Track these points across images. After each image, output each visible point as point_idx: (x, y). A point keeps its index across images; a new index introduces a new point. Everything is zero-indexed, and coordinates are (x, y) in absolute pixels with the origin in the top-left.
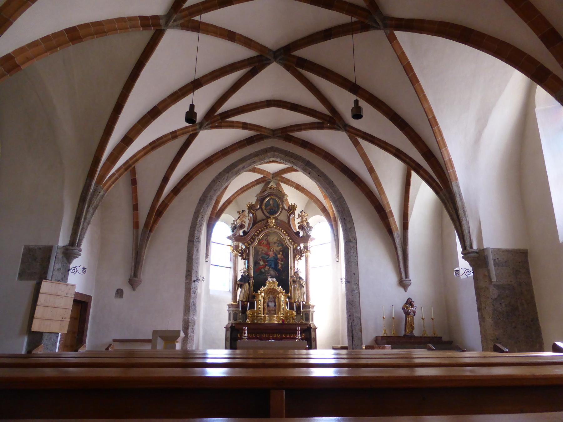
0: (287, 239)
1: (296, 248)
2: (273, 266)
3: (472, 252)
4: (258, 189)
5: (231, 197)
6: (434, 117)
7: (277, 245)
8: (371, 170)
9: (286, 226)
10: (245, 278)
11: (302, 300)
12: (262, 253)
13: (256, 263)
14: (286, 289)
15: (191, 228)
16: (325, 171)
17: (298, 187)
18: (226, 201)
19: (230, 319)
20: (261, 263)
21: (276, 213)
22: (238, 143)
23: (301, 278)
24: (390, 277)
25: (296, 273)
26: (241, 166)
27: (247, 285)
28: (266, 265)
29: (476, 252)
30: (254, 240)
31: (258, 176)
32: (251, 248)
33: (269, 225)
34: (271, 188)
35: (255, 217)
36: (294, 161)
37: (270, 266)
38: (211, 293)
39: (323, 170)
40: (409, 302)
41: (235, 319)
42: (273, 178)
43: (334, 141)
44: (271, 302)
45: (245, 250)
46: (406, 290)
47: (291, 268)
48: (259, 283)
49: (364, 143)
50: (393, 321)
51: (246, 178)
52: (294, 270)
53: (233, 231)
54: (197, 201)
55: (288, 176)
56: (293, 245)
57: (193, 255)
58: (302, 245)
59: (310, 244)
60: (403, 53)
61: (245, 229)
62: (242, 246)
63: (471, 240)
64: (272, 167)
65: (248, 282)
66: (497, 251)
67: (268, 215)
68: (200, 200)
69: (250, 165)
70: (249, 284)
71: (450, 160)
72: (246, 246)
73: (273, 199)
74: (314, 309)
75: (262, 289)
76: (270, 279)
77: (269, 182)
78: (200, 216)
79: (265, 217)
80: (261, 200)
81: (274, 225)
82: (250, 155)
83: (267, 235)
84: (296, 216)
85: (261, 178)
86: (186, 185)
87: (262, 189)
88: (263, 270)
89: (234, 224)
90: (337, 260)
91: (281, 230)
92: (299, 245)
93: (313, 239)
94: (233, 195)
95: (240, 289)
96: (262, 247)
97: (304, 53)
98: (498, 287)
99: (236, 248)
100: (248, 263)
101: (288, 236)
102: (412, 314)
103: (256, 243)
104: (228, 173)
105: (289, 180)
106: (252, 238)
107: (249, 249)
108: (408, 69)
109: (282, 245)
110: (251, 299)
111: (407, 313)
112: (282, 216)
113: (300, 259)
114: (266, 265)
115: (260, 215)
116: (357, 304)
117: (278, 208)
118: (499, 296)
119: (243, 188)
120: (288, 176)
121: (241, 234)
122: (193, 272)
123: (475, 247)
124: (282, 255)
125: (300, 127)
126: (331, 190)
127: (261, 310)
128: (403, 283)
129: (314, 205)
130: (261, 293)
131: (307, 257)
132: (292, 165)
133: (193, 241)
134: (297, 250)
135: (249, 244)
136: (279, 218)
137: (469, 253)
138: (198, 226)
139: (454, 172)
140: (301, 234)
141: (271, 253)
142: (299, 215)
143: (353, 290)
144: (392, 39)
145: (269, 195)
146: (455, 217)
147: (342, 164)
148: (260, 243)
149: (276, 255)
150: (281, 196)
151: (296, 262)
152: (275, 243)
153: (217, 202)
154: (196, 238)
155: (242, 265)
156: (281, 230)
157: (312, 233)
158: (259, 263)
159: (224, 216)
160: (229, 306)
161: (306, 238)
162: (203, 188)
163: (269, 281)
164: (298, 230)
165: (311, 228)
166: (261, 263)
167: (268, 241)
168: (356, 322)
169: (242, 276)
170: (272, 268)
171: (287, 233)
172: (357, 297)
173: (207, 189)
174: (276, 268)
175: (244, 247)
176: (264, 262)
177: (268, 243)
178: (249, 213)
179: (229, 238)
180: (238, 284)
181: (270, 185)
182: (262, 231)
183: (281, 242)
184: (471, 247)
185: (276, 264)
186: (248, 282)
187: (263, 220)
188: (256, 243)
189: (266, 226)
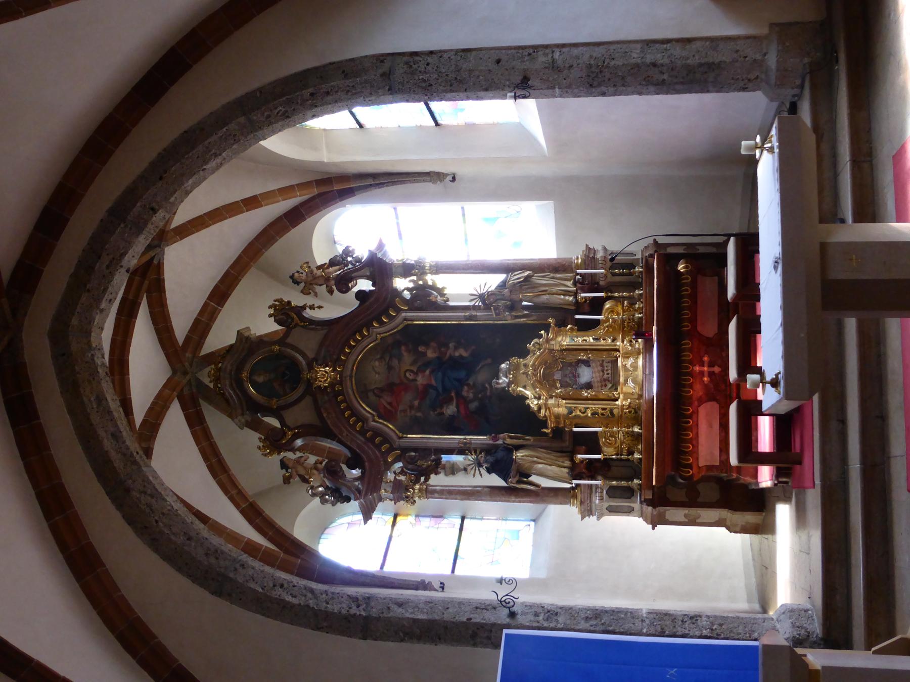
0: (379, 331)
1: (405, 301)
2: (462, 374)
4: (218, 423)
5: (237, 505)
7: (395, 362)
10: (500, 463)
11: (570, 283)
12: (419, 409)
14: (532, 331)
15: (319, 628)
16: (150, 153)
17: (220, 294)
18: (251, 522)
19: (629, 511)
20: (450, 410)
21: (295, 364)
22: (24, 454)
23: (503, 285)
25: (487, 300)
26: (108, 444)
27: (519, 454)
28: (459, 394)
30: (377, 433)
31: (175, 416)
33: (332, 385)
34: (217, 380)
35: (306, 431)
37: (461, 382)
38: (542, 574)
39: (144, 165)
41: (628, 493)
42: (185, 373)
44: (576, 376)
45: (409, 462)
47: (470, 318)
48: (526, 422)
51: (177, 465)
52: (474, 308)
53: (348, 500)
54: (223, 605)
55: (181, 327)
56: (399, 311)
57: (415, 621)
58: (401, 284)
59: (395, 254)
62: (395, 471)
64: (146, 367)
67: (300, 390)
68: (218, 593)
69: (110, 412)
70: (518, 448)
73: (252, 373)
74: (598, 247)
75: (533, 404)
76: (503, 380)
77: (200, 383)
78: (278, 593)
79: (308, 399)
80: (249, 412)
81: (334, 370)
82: (71, 412)
83: (364, 393)
84: (308, 300)
85: (184, 408)
86: (160, 645)
87: (217, 407)
88: (474, 406)
89: (322, 496)
90: (450, 178)
91: (351, 347)
92: (397, 293)
93: (381, 246)
94: (232, 499)
95: (533, 478)
96: (401, 407)
99: (401, 493)
101: (369, 325)
104: (128, 490)
105: (197, 322)
106: (371, 440)
107: (405, 450)
109: (398, 344)
110: (567, 442)
112: (308, 343)
113: (440, 292)
114: (459, 394)
115: (301, 414)
116: (598, 52)
117: (280, 356)
119: (211, 468)
120: (181, 327)
121: (356, 472)
122: (477, 618)
124: (427, 345)
126: (214, 138)
127: (597, 406)
129: (277, 250)
130: (547, 408)
131: (439, 269)
132: (123, 270)
133: (367, 619)
134: (414, 297)
135: (391, 449)
136: (311, 355)
138: (312, 603)
140: (365, 285)
141: (421, 380)
142: (305, 292)
143: (553, 66)
145: (239, 384)
146: (370, 181)
148: (388, 415)
149: (427, 364)
150: (247, 344)
151: (451, 304)
152: (390, 368)
153: (250, 548)
154: (354, 610)
156: (351, 347)
157: (362, 252)
158: (452, 418)
159: (300, 533)
160: (587, 511)
161: (378, 268)
162: (180, 583)
163: (509, 384)
165: (347, 252)
166: (450, 410)
167: (382, 390)
168: (659, 58)
169: (489, 471)
170: (468, 376)
172: (576, 51)
173: (179, 570)
175: (399, 465)
176: (449, 401)
177: (391, 388)
178: (293, 450)
179: (367, 515)
180: (516, 487)
181: (206, 381)
182: (349, 407)
183: (388, 349)
185: (456, 363)
187: (315, 401)
189: (335, 391)
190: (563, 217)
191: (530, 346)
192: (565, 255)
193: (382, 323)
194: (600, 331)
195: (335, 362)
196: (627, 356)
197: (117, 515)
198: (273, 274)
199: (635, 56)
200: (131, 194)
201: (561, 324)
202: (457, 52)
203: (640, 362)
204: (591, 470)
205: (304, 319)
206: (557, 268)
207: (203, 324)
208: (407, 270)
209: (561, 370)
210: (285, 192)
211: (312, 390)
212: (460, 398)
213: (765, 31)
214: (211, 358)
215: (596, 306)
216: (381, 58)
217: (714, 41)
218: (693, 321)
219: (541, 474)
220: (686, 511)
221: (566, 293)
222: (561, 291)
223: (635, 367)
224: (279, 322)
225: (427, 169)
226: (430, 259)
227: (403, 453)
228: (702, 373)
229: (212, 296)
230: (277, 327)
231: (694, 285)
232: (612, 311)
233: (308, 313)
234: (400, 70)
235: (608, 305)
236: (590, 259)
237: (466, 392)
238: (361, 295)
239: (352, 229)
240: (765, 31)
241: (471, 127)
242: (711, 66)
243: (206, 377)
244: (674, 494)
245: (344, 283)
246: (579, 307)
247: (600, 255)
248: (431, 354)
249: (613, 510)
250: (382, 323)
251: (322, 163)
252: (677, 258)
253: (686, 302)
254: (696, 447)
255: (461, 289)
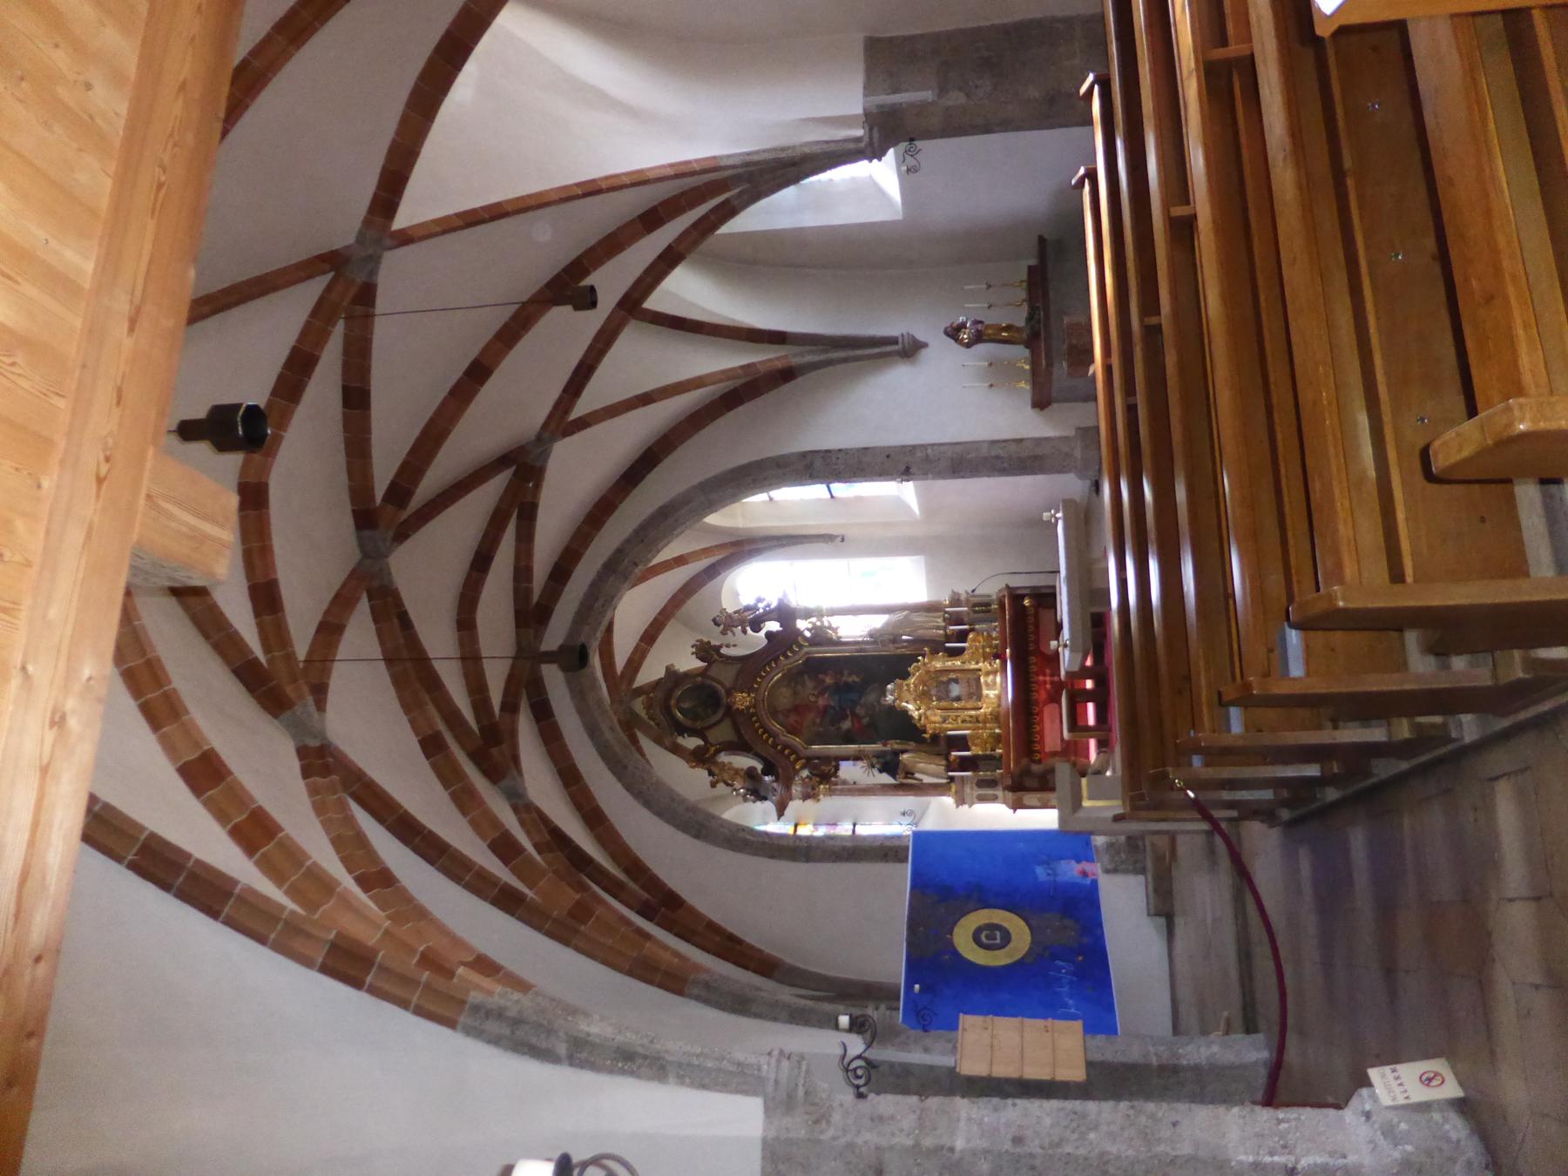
3: (871, 138)
6: (578, 185)
8: (646, 399)
9: (752, 666)
10: (889, 764)
13: (848, 739)
17: (649, 637)
19: (994, 799)
20: (846, 725)
24: (898, 378)
27: (905, 756)
29: (871, 130)
30: (786, 746)
32: (808, 753)
36: (601, 601)
40: (954, 333)
41: (992, 783)
43: (575, 475)
44: (948, 692)
46: (924, 345)
48: (907, 729)
49: (581, 408)
50: (997, 375)
53: (764, 798)
58: (802, 625)
59: (797, 601)
60: (436, 222)
61: (759, 767)
63: (845, 141)
65: (897, 753)
66: (869, 89)
67: (721, 713)
71: (671, 165)
72: (803, 767)
73: (678, 701)
75: (916, 714)
76: (890, 698)
78: (741, 835)
83: (774, 713)
88: (865, 721)
89: (744, 796)
92: (800, 633)
97: (383, 473)
98: (943, 90)
100: (846, 759)
102: (980, 327)
103: (797, 741)
104: (625, 767)
107: (809, 759)
108: (472, 219)
110: (941, 745)
111: (978, 338)
113: (835, 630)
115: (723, 732)
116: (958, 449)
117: (702, 686)
118: (960, 89)
120: (620, 661)
123: (859, 132)
124: (825, 673)
125: (522, 572)
128: (909, 350)
129: (691, 605)
131: (834, 612)
136: (728, 683)
137: (871, 143)
139: (697, 161)
140: (773, 626)
141: (821, 702)
143: (927, 459)
144: (405, 238)
145: (667, 710)
147: (617, 483)
148: (793, 731)
152: (795, 693)
155: (850, 771)
158: (848, 731)
160: (961, 801)
161: (785, 614)
162: (667, 830)
164: (762, 634)
166: (846, 725)
168: (1001, 453)
171: (769, 664)
174: (861, 689)
175: (805, 773)
176: (844, 718)
177: (797, 709)
183: (794, 677)
184: (858, 140)
185: (849, 687)
186: (897, 753)
188: (797, 741)
189: (747, 715)
190: (933, 573)
191: (911, 669)
192: (934, 598)
193: (787, 657)
194: (966, 656)
195: (750, 690)
196: (988, 674)
197: (619, 786)
198: (689, 624)
199: (984, 451)
200: (619, 553)
201: (935, 652)
202: (858, 450)
203: (998, 679)
204: (964, 764)
205: (722, 656)
206: (931, 608)
207: (635, 663)
208: (807, 614)
209: (938, 686)
210: (706, 552)
211: (730, 712)
212: (854, 714)
213: (1073, 433)
214: (639, 692)
215: (962, 636)
216: (804, 455)
217: (1038, 441)
218: (1037, 642)
219: (923, 772)
220: (1039, 795)
221: (938, 628)
222: (934, 627)
223: (994, 682)
224: (702, 660)
225: (822, 532)
226: (826, 605)
227: (809, 762)
228: (1045, 683)
229: (643, 639)
230: (700, 664)
231: (1036, 615)
232: (974, 640)
233: (724, 651)
234: (818, 463)
235: (971, 636)
236: (956, 601)
237: (860, 711)
238: (769, 635)
239: (753, 584)
240: (1071, 433)
241: (859, 499)
242: (1036, 458)
243: (639, 706)
244: (1028, 782)
245: (756, 625)
246: (949, 638)
247: (963, 597)
248: (829, 680)
249: (982, 799)
250: (787, 657)
251: (738, 529)
252: (1023, 597)
253: (1031, 628)
254: (1042, 737)
255: (853, 629)
